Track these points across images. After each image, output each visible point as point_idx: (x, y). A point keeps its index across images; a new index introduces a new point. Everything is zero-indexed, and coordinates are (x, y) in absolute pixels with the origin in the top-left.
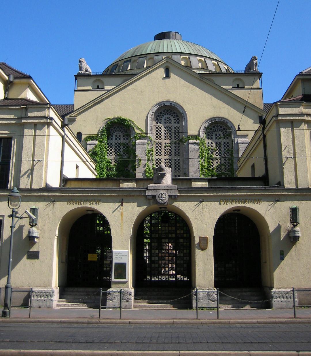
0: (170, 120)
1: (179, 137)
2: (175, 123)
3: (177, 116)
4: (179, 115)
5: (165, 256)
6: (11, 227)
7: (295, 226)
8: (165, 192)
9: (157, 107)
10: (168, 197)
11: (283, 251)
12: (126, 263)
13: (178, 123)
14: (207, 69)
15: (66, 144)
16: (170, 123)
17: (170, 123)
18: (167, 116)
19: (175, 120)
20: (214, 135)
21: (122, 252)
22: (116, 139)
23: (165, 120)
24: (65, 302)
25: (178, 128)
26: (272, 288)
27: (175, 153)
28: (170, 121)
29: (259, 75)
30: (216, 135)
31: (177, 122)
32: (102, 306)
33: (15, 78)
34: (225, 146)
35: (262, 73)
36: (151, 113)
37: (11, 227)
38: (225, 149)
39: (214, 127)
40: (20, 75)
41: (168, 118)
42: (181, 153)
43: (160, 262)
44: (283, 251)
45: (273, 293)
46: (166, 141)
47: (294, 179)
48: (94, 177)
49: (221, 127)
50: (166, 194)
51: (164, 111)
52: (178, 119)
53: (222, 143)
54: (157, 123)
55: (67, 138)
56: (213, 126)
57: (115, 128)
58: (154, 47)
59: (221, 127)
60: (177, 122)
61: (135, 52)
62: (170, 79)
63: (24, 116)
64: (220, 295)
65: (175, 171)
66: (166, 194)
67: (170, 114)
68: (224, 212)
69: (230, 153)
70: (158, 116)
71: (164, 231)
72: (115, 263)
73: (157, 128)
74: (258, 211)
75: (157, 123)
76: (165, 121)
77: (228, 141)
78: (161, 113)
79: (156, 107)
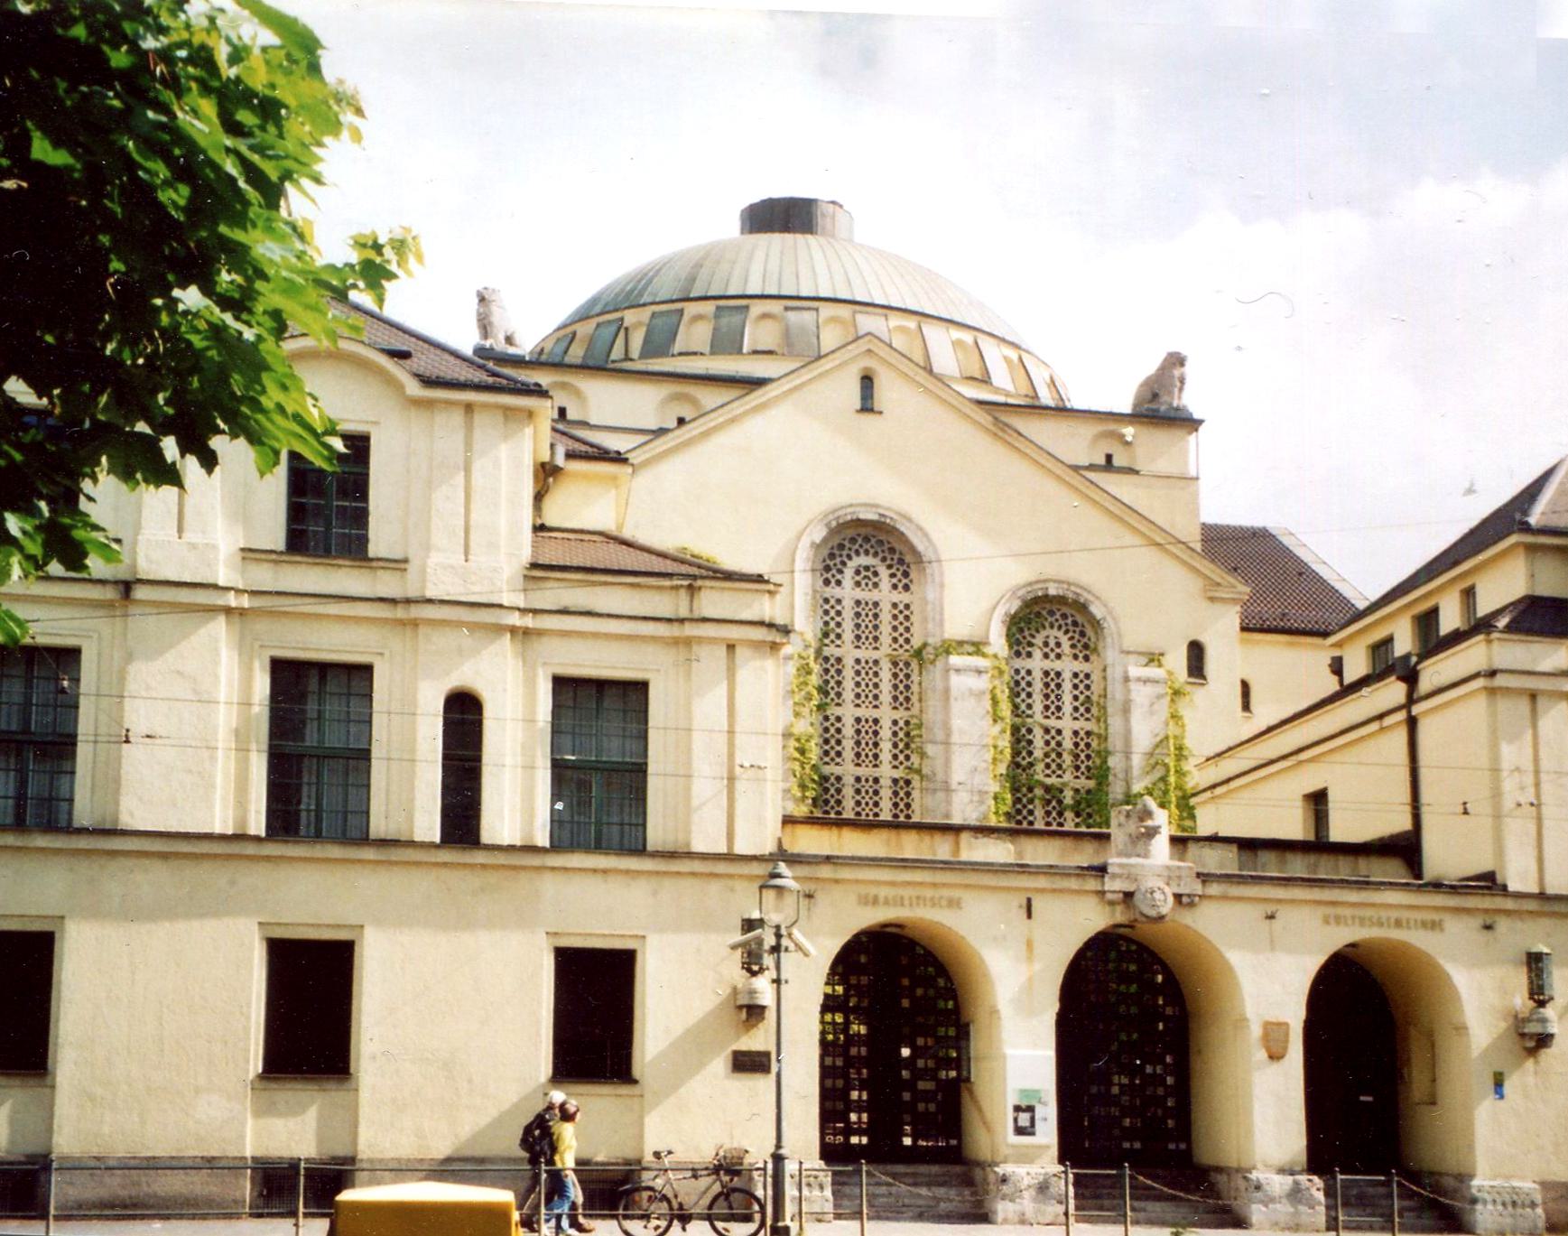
0: (876, 574)
1: (907, 641)
3: (901, 561)
4: (908, 558)
6: (774, 981)
7: (1542, 1004)
8: (1162, 885)
10: (1171, 899)
11: (1501, 1074)
13: (906, 588)
14: (985, 380)
16: (876, 585)
18: (864, 560)
19: (893, 575)
26: (1472, 1177)
27: (895, 698)
29: (1189, 423)
30: (1046, 644)
32: (305, 1207)
33: (570, 455)
34: (1076, 687)
36: (805, 543)
37: (774, 981)
38: (1076, 698)
40: (584, 448)
41: (867, 568)
43: (943, 1074)
44: (1501, 1074)
45: (1474, 1191)
47: (1533, 866)
49: (1064, 616)
50: (1167, 889)
51: (853, 540)
52: (906, 574)
53: (1067, 675)
54: (827, 582)
58: (773, 266)
59: (1064, 616)
61: (692, 280)
62: (354, 232)
63: (684, 613)
64: (838, 1182)
67: (876, 555)
69: (1094, 710)
70: (832, 556)
71: (1132, 1014)
73: (826, 601)
75: (827, 582)
77: (1086, 667)
78: (841, 547)
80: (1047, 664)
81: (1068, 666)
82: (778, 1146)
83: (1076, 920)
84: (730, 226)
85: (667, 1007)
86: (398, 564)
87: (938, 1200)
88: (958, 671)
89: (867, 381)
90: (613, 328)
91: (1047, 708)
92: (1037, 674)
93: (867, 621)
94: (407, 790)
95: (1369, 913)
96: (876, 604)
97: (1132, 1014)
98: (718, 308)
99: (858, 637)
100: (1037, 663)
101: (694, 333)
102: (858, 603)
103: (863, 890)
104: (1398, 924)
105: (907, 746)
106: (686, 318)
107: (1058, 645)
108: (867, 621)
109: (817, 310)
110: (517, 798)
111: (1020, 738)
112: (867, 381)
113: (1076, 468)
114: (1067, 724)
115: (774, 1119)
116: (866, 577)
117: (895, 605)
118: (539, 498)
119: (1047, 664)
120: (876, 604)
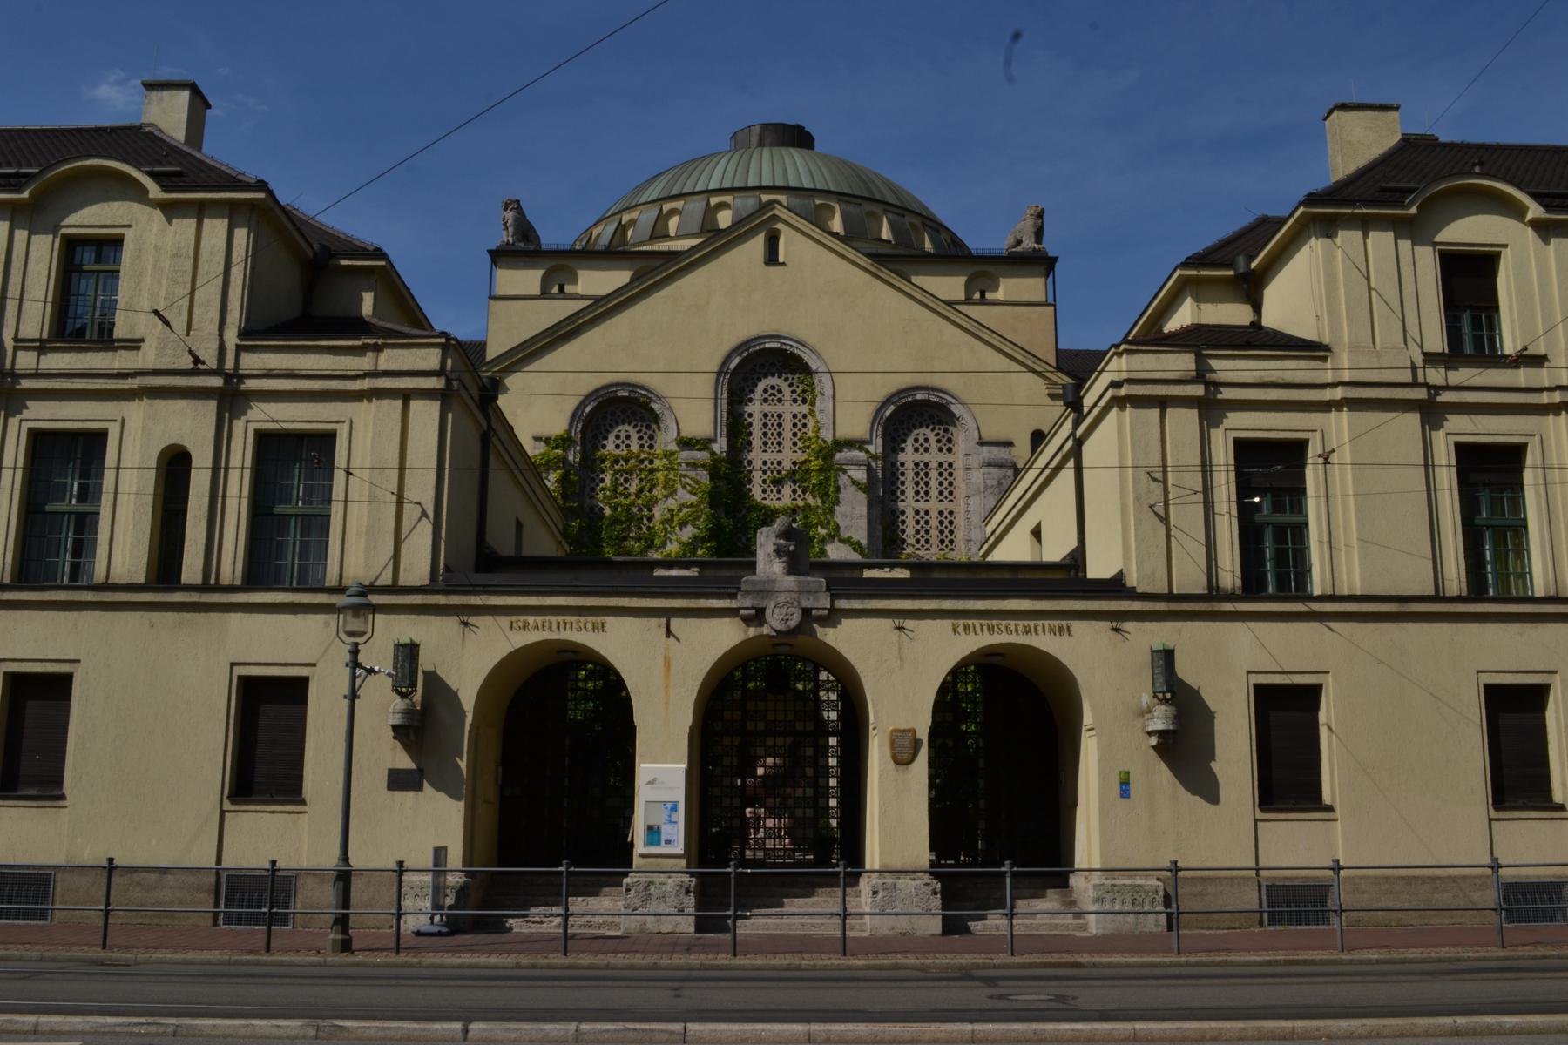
0: (780, 391)
12: (389, 788)
15: (1068, 474)
16: (780, 400)
17: (780, 400)
22: (916, 450)
23: (765, 391)
35: (1055, 259)
41: (773, 387)
46: (766, 457)
48: (561, 554)
53: (934, 465)
55: (497, 442)
57: (613, 414)
68: (727, 654)
71: (776, 723)
74: (848, 656)
80: (918, 457)
82: (345, 858)
83: (713, 638)
86: (134, 344)
87: (633, 911)
91: (917, 493)
93: (771, 430)
94: (123, 546)
96: (780, 416)
97: (776, 723)
99: (765, 443)
102: (765, 415)
104: (1027, 631)
107: (926, 440)
108: (771, 430)
110: (220, 533)
113: (950, 303)
114: (934, 505)
115: (424, 833)
117: (795, 416)
119: (918, 457)
120: (780, 416)
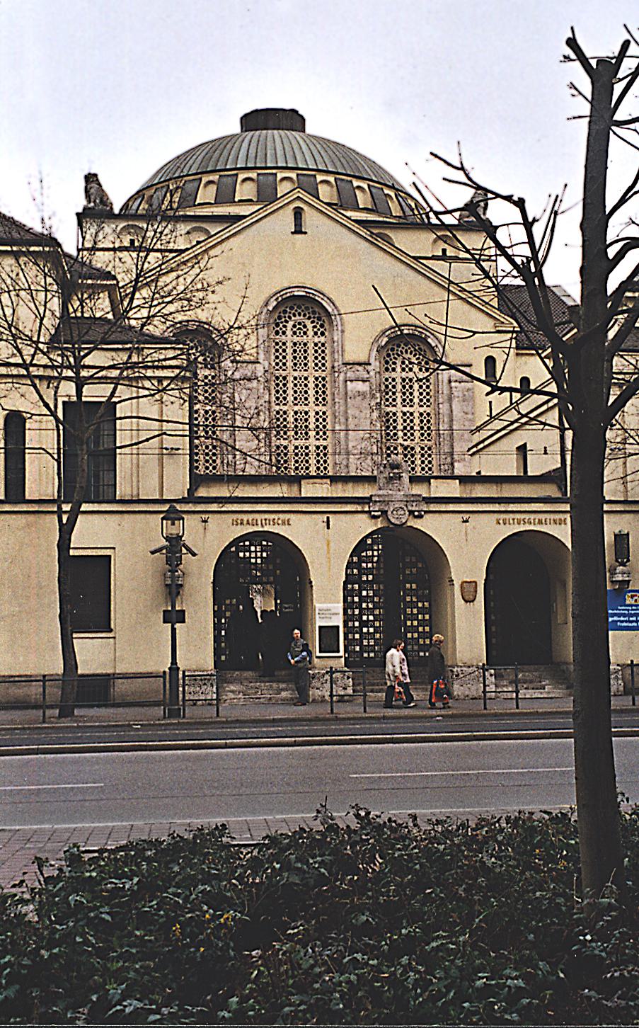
2: (316, 333)
5: (373, 621)
9: (277, 298)
15: (547, 398)
16: (305, 333)
20: (399, 362)
21: (328, 607)
23: (294, 326)
24: (285, 702)
25: (323, 345)
28: (305, 330)
31: (319, 332)
39: (392, 350)
42: (329, 399)
50: (405, 508)
56: (397, 342)
60: (319, 332)
65: (317, 437)
66: (405, 508)
72: (320, 627)
76: (295, 329)
79: (275, 298)
81: (310, 339)
84: (236, 129)
85: (131, 587)
88: (351, 381)
89: (298, 213)
90: (165, 190)
92: (399, 380)
93: (300, 355)
95: (245, 517)
97: (399, 569)
98: (220, 176)
100: (398, 374)
101: (206, 194)
103: (235, 516)
104: (540, 522)
105: (388, 421)
106: (203, 182)
108: (300, 355)
109: (276, 174)
111: (388, 420)
112: (298, 213)
116: (300, 329)
118: (508, 198)
